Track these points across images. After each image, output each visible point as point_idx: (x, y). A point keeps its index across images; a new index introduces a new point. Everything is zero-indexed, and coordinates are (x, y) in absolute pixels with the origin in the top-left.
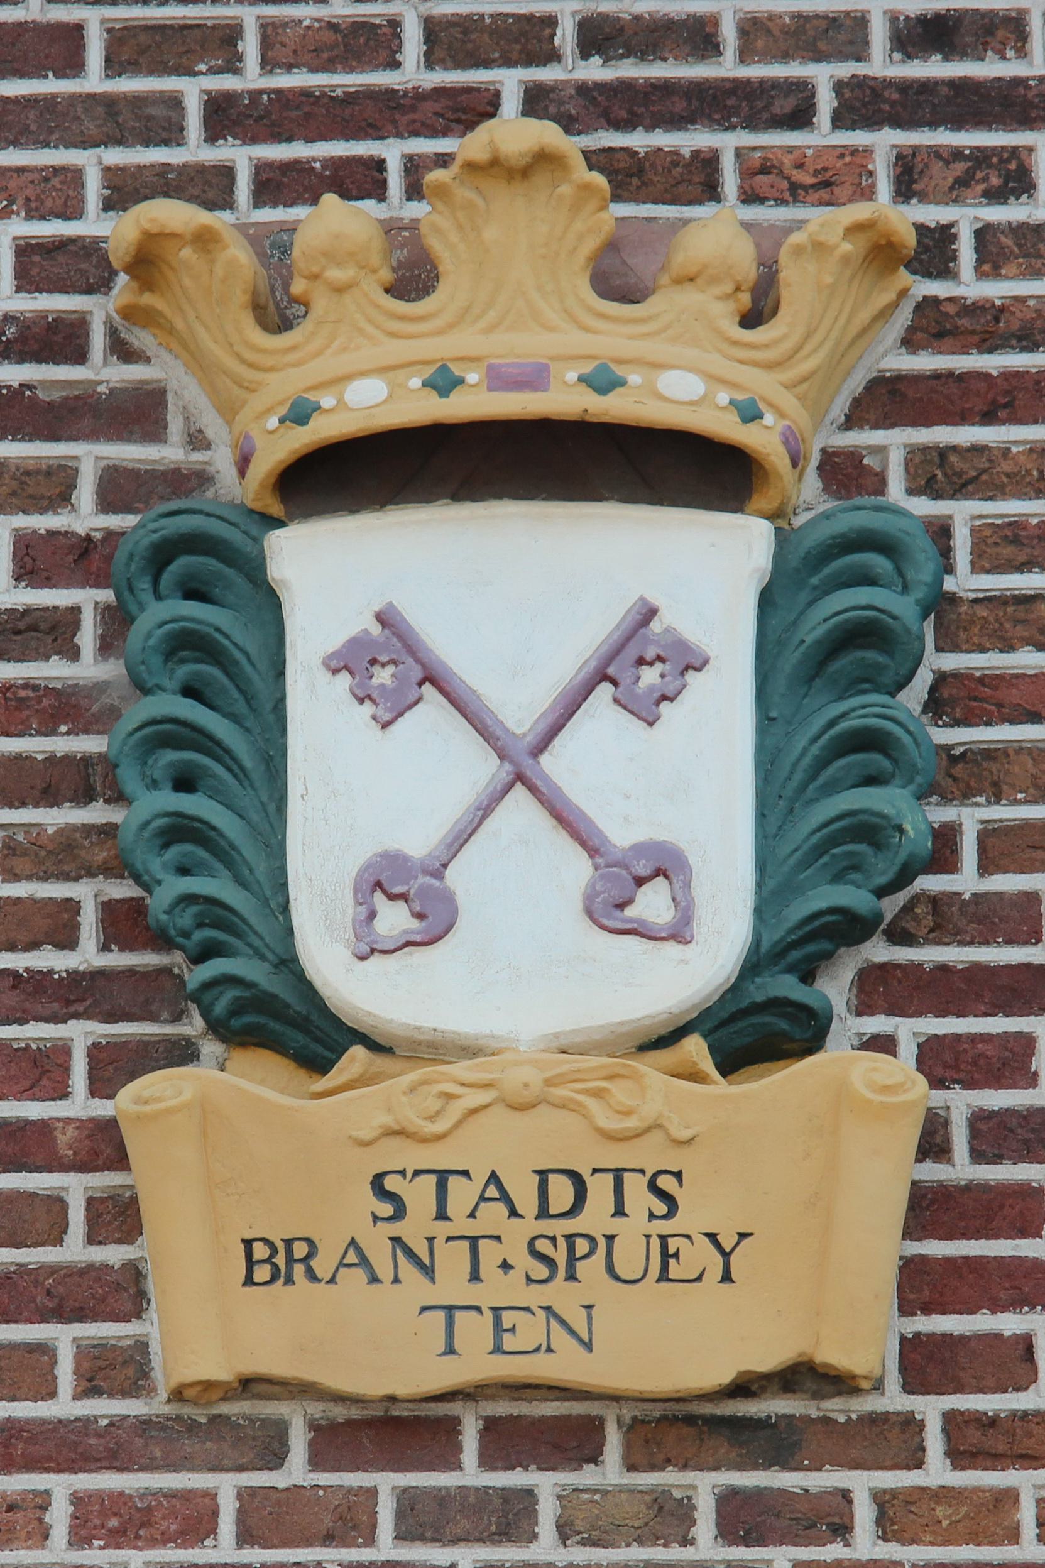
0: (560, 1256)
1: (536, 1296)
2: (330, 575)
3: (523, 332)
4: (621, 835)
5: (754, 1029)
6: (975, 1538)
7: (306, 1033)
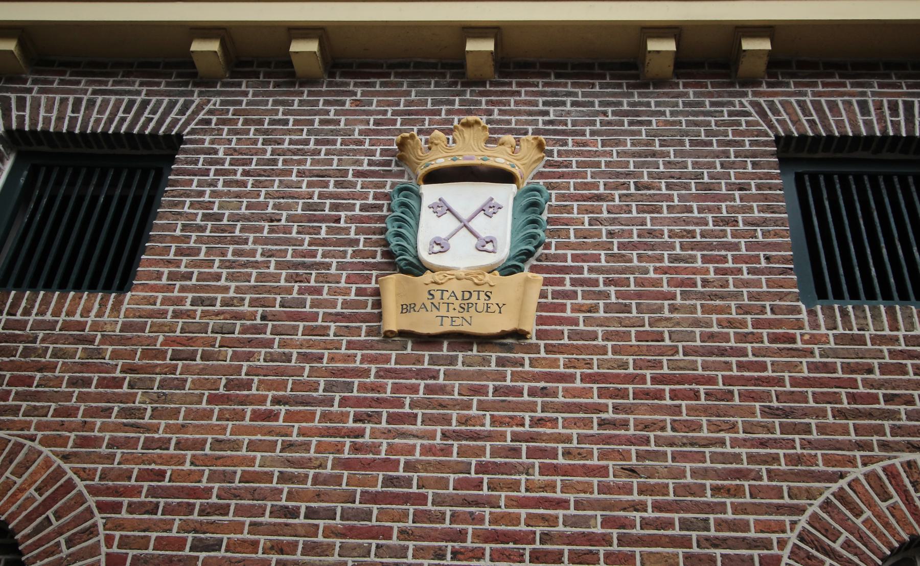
0: (466, 307)
1: (460, 315)
2: (430, 193)
3: (470, 149)
4: (483, 235)
5: (508, 269)
6: (550, 367)
7: (417, 268)
